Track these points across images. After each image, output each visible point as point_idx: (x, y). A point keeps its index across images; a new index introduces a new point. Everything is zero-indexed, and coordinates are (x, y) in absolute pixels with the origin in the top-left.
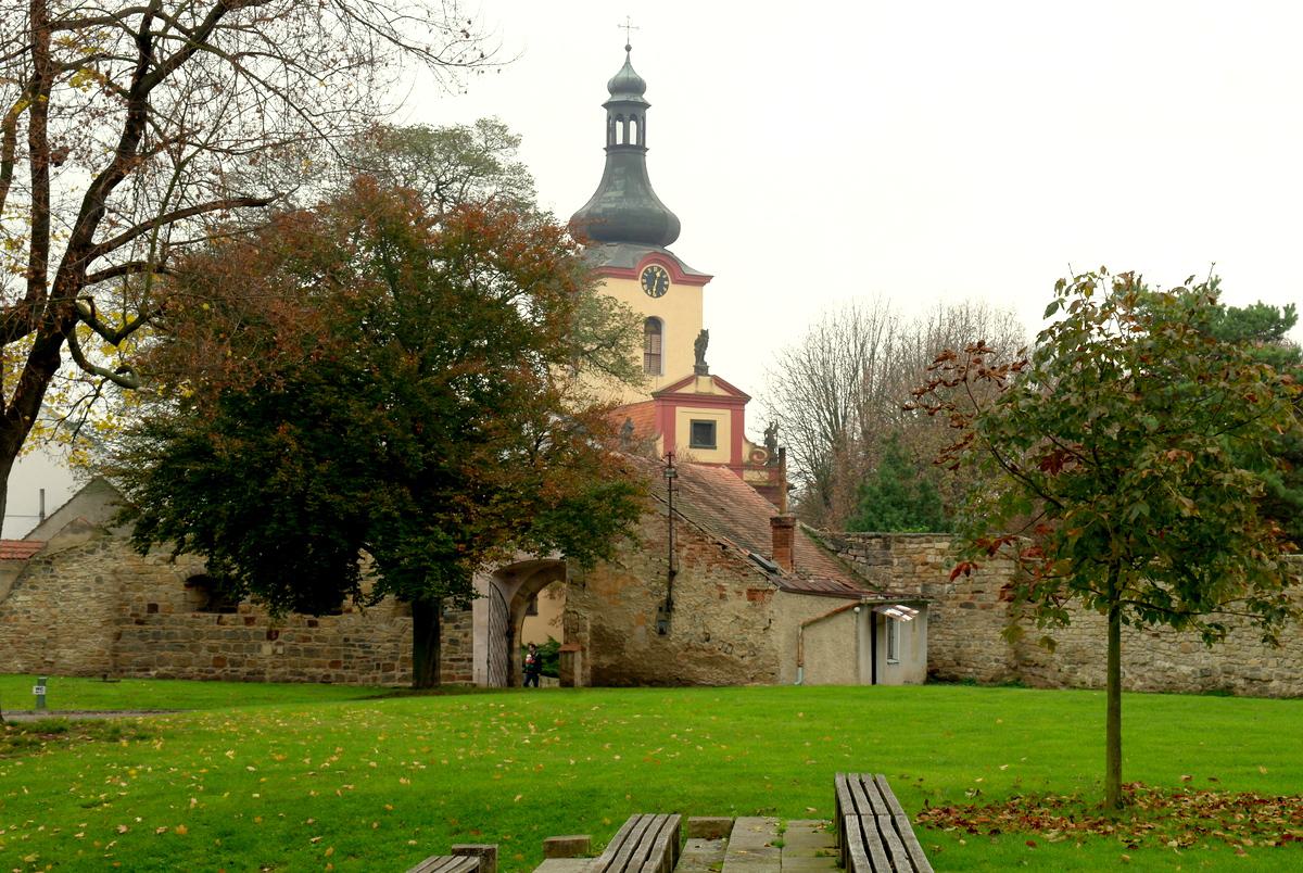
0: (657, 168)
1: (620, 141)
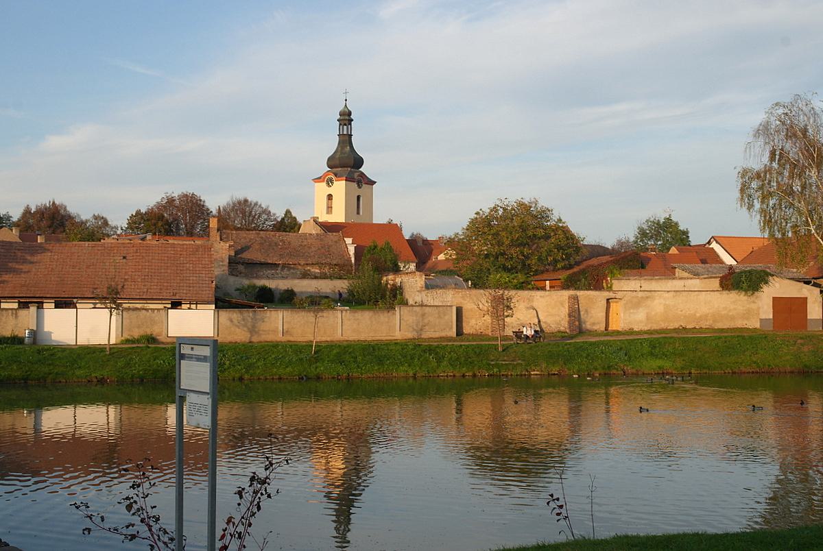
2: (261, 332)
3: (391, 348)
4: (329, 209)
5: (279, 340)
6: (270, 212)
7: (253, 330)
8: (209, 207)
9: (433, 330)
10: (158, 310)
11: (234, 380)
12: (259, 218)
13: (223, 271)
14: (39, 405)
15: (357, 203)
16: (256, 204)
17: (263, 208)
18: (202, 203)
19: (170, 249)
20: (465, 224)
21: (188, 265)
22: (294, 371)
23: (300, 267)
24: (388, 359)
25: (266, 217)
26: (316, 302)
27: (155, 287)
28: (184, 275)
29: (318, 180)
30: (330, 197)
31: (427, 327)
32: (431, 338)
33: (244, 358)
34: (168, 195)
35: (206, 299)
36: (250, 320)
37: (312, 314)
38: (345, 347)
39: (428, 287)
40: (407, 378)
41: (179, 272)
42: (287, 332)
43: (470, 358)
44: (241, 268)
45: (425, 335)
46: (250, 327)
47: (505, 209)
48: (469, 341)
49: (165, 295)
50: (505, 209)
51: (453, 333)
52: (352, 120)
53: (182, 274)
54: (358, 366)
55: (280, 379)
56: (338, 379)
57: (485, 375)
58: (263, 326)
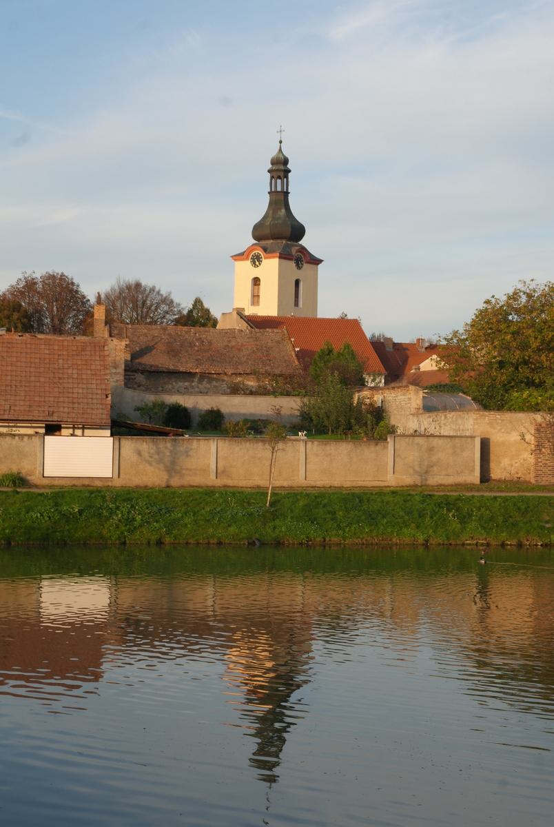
0: (293, 201)
1: (273, 190)
2: (184, 472)
3: (386, 498)
4: (255, 298)
5: (210, 484)
6: (172, 302)
7: (172, 469)
8: (86, 293)
9: (444, 473)
10: (30, 436)
11: (149, 543)
12: (156, 310)
13: (117, 381)
14: (34, 574)
15: (295, 290)
16: (153, 290)
17: (162, 295)
18: (75, 288)
19: (43, 347)
20: (469, 316)
21: (70, 371)
22: (241, 532)
23: (226, 378)
24: (384, 517)
25: (166, 308)
26: (255, 428)
27: (22, 403)
28: (66, 385)
29: (239, 257)
30: (256, 281)
31: (435, 469)
32: (441, 485)
33: (164, 511)
34: (27, 276)
35: (98, 421)
36: (168, 454)
37: (267, 446)
38: (316, 497)
39: (428, 408)
40: (414, 546)
41: (56, 380)
42: (223, 472)
43: (510, 517)
44: (140, 378)
45: (433, 480)
46: (168, 464)
47: (529, 296)
48: (501, 491)
49: (36, 415)
50: (529, 296)
51: (475, 477)
52: (290, 171)
53: (61, 384)
54: (339, 526)
55: (220, 544)
56: (308, 545)
57: (536, 545)
58: (188, 463)
